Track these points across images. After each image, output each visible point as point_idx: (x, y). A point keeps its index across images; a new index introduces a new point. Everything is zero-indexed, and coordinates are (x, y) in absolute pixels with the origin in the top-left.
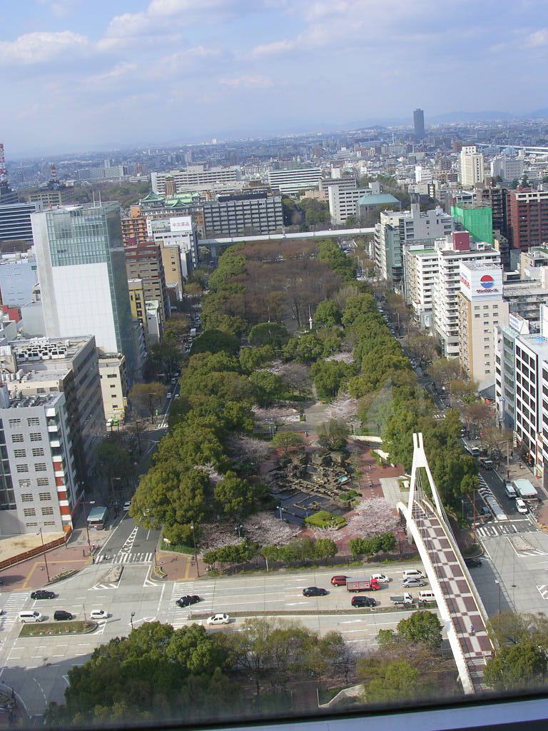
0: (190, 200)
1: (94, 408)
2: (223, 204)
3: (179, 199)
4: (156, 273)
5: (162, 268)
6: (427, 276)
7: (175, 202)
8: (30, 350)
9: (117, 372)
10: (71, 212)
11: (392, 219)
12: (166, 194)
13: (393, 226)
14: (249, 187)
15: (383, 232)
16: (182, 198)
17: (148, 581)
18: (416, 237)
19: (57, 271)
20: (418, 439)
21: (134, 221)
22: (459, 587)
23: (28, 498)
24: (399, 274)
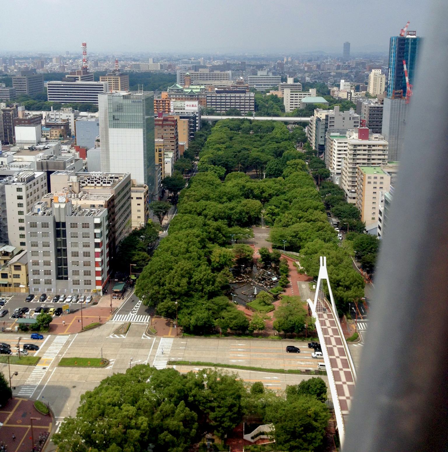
0: (198, 90)
1: (126, 218)
2: (219, 95)
3: (192, 89)
4: (173, 136)
5: (177, 132)
6: (340, 152)
7: (189, 91)
8: (89, 179)
9: (142, 195)
10: (123, 96)
11: (321, 114)
12: (185, 85)
13: (321, 119)
14: (236, 85)
15: (315, 122)
16: (194, 89)
17: (145, 335)
18: (335, 127)
19: (113, 132)
20: (323, 260)
21: (163, 101)
22: (343, 363)
23: (76, 273)
24: (322, 149)
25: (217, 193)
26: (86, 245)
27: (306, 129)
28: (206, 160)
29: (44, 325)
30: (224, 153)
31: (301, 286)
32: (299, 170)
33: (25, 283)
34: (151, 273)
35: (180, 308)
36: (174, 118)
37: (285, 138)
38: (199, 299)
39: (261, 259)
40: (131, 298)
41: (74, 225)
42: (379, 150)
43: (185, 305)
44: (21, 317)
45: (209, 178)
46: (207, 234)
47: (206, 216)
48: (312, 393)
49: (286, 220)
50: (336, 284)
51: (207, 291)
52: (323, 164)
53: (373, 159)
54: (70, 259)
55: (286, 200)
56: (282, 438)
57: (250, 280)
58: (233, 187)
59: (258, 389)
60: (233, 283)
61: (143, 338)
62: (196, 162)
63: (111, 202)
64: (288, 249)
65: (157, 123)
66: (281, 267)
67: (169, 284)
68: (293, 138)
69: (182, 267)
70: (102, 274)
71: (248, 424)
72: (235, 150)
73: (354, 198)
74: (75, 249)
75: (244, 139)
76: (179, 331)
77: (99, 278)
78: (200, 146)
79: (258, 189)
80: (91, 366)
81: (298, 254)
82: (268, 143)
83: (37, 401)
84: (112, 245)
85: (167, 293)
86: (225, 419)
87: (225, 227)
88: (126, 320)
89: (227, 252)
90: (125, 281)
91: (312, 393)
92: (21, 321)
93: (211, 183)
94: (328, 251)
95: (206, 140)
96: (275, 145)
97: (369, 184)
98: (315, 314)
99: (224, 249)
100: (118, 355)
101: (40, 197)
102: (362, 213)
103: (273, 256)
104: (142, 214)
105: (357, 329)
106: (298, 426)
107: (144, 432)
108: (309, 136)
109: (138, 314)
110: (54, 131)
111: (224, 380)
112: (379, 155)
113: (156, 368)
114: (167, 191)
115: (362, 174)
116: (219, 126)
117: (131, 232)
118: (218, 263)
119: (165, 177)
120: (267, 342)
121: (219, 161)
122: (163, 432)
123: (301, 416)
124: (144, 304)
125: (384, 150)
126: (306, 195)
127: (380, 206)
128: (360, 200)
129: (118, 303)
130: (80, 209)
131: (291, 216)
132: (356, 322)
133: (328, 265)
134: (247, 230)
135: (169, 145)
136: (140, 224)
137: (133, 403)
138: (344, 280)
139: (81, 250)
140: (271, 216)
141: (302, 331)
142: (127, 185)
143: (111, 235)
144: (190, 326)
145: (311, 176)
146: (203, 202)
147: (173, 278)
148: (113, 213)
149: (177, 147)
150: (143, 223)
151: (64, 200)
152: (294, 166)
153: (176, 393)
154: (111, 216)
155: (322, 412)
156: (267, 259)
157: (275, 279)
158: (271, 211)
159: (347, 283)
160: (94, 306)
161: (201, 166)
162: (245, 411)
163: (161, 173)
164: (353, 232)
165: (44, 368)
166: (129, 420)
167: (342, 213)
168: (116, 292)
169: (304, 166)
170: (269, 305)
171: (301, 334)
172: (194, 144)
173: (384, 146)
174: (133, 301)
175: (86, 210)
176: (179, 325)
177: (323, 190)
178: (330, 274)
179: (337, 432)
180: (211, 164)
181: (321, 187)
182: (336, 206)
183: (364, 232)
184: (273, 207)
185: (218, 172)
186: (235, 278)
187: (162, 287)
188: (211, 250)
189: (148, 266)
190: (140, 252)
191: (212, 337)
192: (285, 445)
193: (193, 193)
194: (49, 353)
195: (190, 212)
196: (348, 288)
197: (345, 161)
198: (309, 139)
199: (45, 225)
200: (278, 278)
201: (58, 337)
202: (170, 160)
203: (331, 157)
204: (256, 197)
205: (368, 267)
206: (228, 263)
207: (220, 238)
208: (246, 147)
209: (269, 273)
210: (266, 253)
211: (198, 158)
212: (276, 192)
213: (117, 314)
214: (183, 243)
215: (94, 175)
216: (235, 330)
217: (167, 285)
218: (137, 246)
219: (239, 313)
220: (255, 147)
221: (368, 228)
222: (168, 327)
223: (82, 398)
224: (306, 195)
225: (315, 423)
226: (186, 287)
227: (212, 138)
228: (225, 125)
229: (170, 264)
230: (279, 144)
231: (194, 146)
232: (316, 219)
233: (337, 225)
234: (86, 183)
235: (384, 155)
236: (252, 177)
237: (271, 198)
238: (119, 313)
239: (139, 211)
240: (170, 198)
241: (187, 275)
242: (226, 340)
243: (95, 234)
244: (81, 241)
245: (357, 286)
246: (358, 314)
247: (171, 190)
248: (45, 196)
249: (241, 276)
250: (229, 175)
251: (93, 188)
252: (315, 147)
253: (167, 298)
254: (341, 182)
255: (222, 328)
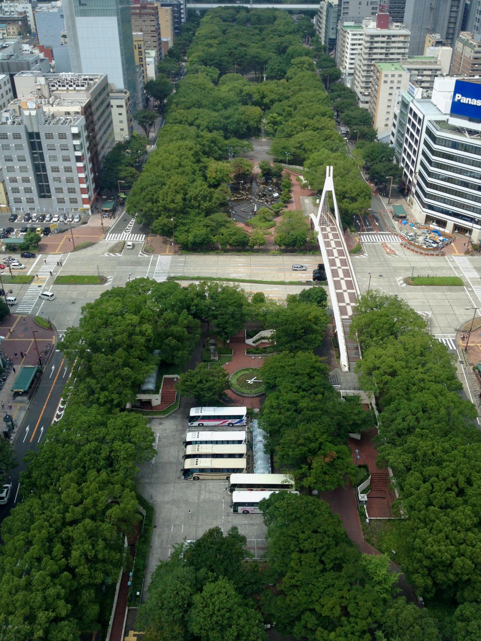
4: (154, 29)
5: (158, 24)
6: (354, 47)
9: (123, 102)
13: (333, 4)
19: (81, 22)
20: (330, 170)
24: (332, 43)
25: (211, 100)
26: (67, 159)
27: (314, 20)
28: (195, 60)
29: (33, 245)
30: (217, 50)
31: (303, 201)
32: (305, 70)
33: (6, 202)
34: (142, 189)
35: (176, 226)
36: (153, 4)
37: (289, 30)
38: (196, 216)
39: (262, 174)
40: (123, 218)
41: (49, 136)
42: (399, 42)
43: (181, 223)
44: (7, 237)
45: (200, 81)
46: (201, 146)
47: (198, 126)
48: (313, 300)
49: (290, 129)
50: (341, 196)
51: (204, 208)
52: (333, 63)
53: (392, 54)
54: (51, 175)
55: (289, 106)
56: (284, 339)
57: (250, 196)
58: (229, 91)
59: (259, 298)
60: (231, 201)
61: (139, 256)
62: (184, 64)
63: (88, 109)
64: (291, 163)
65: (132, 11)
66: (283, 182)
67: (163, 200)
68: (298, 31)
69: (176, 182)
70: (88, 191)
71: (250, 330)
72: (230, 46)
73: (367, 102)
74: (54, 164)
75: (241, 33)
76: (177, 249)
77: (86, 196)
78: (187, 43)
79: (258, 94)
80: (88, 283)
81: (301, 168)
82: (269, 37)
83: (38, 317)
84: (95, 159)
85: (162, 210)
86: (228, 326)
87: (221, 139)
88: (120, 239)
89: (224, 167)
90: (114, 199)
91: (313, 300)
92: (7, 241)
93: (203, 87)
94: (335, 161)
95: (194, 35)
96: (277, 40)
97: (386, 84)
98: (317, 228)
99: (220, 163)
100: (115, 273)
101: (6, 105)
102: (374, 119)
103: (274, 170)
104: (125, 125)
105: (361, 241)
106: (299, 328)
107: (149, 338)
108: (317, 28)
109: (132, 233)
110: (11, 28)
111: (225, 290)
112: (399, 48)
113: (156, 282)
114: (152, 99)
115: (378, 71)
116: (209, 17)
117: (114, 145)
118: (214, 178)
119: (149, 80)
120: (268, 257)
121: (211, 61)
122: (167, 338)
123: (302, 320)
124: (138, 222)
125: (405, 42)
126: (313, 99)
127: (396, 108)
128: (374, 104)
129: (110, 223)
130: (53, 116)
131: (295, 124)
132: (360, 235)
133: (334, 177)
134: (245, 142)
135: (151, 41)
136: (124, 138)
137: (135, 313)
138: (351, 191)
139: (62, 165)
140: (272, 125)
141: (304, 244)
142: (104, 89)
143: (92, 149)
144: (188, 244)
145: (319, 77)
146: (195, 110)
147: (167, 194)
148: (92, 122)
149: (160, 44)
150: (128, 137)
151: (34, 106)
152: (299, 65)
153: (178, 303)
154: (90, 126)
155: (322, 316)
156: (267, 174)
157: (276, 195)
158: (272, 119)
159: (354, 195)
160: (84, 225)
161: (190, 68)
162: (248, 318)
163: (143, 76)
164: (363, 141)
165: (40, 286)
166: (133, 328)
167: (352, 120)
168: (106, 211)
169: (310, 64)
170: (270, 221)
171: (303, 248)
172: (180, 40)
173: (405, 36)
174: (125, 220)
175: (61, 118)
176: (176, 243)
177: (332, 94)
178: (336, 185)
179: (336, 335)
180: (201, 65)
181: (330, 91)
182: (346, 112)
183: (375, 140)
184: (275, 115)
185: (210, 74)
186: (233, 195)
187: (155, 204)
188: (206, 164)
189: (138, 182)
190: (127, 168)
191: (211, 253)
192: (286, 346)
193: (182, 99)
194: (43, 272)
195: (180, 122)
196: (354, 200)
197: (360, 57)
198: (317, 32)
199: (17, 136)
200: (280, 194)
201: (49, 256)
202: (152, 60)
203: (343, 54)
204: (256, 104)
205: (377, 178)
206: (226, 179)
207: (216, 152)
208: (244, 42)
209: (270, 189)
210: (267, 167)
211: (186, 58)
212: (278, 96)
213: (110, 233)
214: (174, 156)
215: (64, 76)
216: (235, 246)
217: (161, 201)
218: (123, 161)
219: (239, 229)
220: (253, 43)
221: (380, 136)
222: (164, 245)
223: (83, 309)
224: (313, 99)
225: (315, 327)
226: (181, 204)
227: (202, 31)
228: (216, 15)
229: (162, 179)
230: (282, 38)
231: (180, 42)
232: (323, 127)
233: (347, 134)
234: (57, 86)
235: (405, 48)
236: (251, 80)
237: (272, 105)
238: (111, 233)
239: (121, 122)
240: (156, 106)
241: (182, 191)
242: (225, 256)
243: (74, 146)
244: (60, 154)
245: (364, 197)
246: (363, 227)
247: (157, 97)
248: (12, 102)
249: (239, 193)
250: (223, 77)
251: (65, 92)
252: (325, 42)
253: (162, 216)
254: (353, 84)
255: (221, 245)
